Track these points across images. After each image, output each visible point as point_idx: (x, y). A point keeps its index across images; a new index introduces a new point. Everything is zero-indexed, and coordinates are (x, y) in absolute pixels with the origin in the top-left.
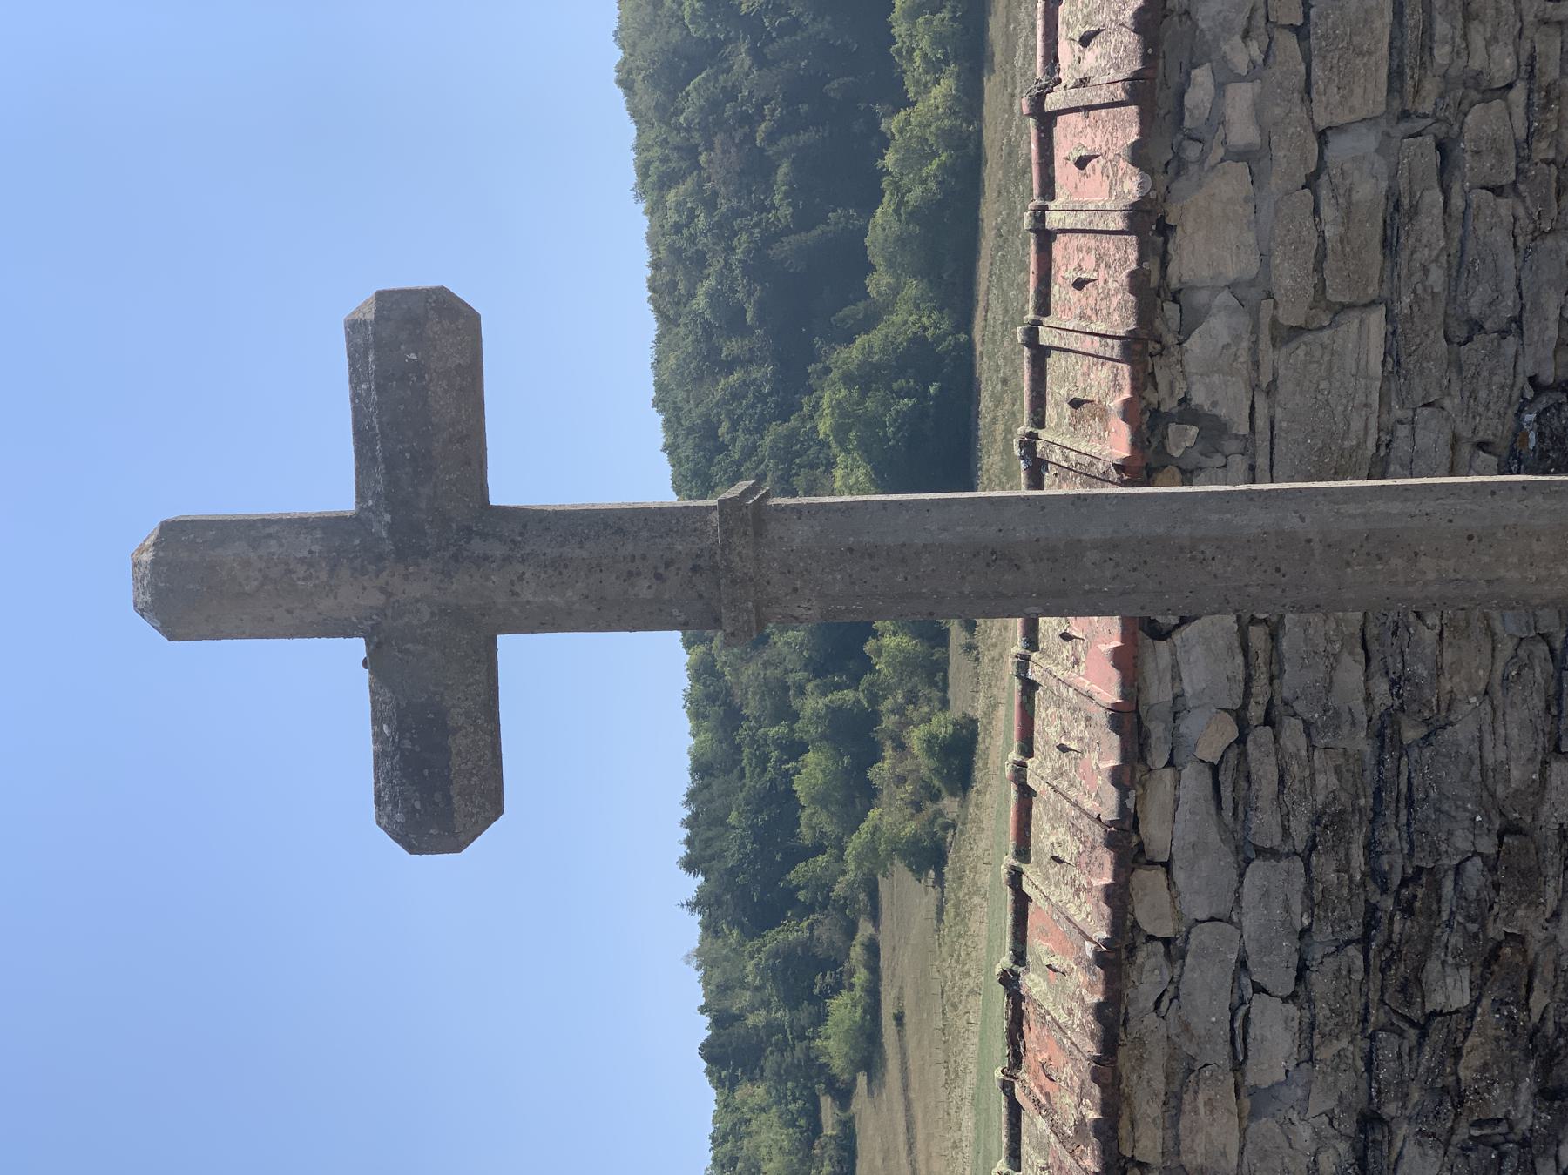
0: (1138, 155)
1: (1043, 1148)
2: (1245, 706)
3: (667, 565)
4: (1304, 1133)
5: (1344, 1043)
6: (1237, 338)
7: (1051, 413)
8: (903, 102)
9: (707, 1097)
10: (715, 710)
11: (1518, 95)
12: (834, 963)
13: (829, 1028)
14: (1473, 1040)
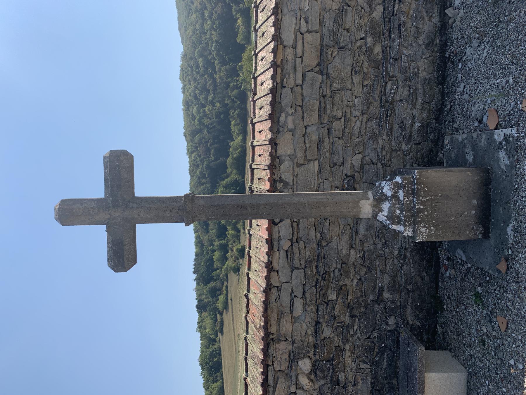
0: (271, 129)
1: (253, 330)
2: (292, 239)
3: (173, 209)
4: (305, 326)
5: (312, 307)
6: (290, 166)
7: (254, 181)
8: (233, 140)
9: (197, 315)
10: (199, 245)
11: (343, 120)
12: (220, 290)
13: (219, 302)
14: (337, 306)
